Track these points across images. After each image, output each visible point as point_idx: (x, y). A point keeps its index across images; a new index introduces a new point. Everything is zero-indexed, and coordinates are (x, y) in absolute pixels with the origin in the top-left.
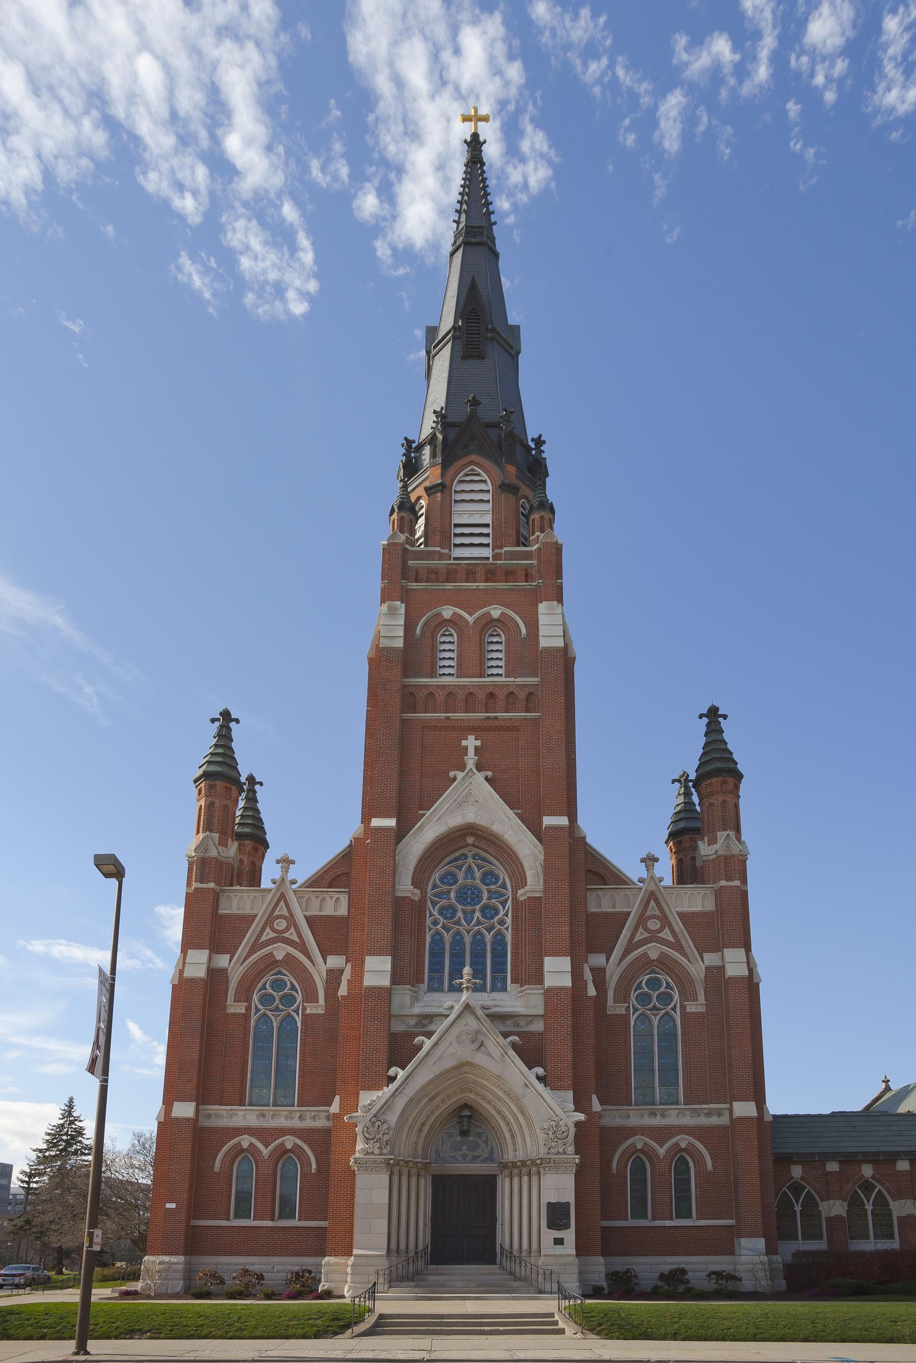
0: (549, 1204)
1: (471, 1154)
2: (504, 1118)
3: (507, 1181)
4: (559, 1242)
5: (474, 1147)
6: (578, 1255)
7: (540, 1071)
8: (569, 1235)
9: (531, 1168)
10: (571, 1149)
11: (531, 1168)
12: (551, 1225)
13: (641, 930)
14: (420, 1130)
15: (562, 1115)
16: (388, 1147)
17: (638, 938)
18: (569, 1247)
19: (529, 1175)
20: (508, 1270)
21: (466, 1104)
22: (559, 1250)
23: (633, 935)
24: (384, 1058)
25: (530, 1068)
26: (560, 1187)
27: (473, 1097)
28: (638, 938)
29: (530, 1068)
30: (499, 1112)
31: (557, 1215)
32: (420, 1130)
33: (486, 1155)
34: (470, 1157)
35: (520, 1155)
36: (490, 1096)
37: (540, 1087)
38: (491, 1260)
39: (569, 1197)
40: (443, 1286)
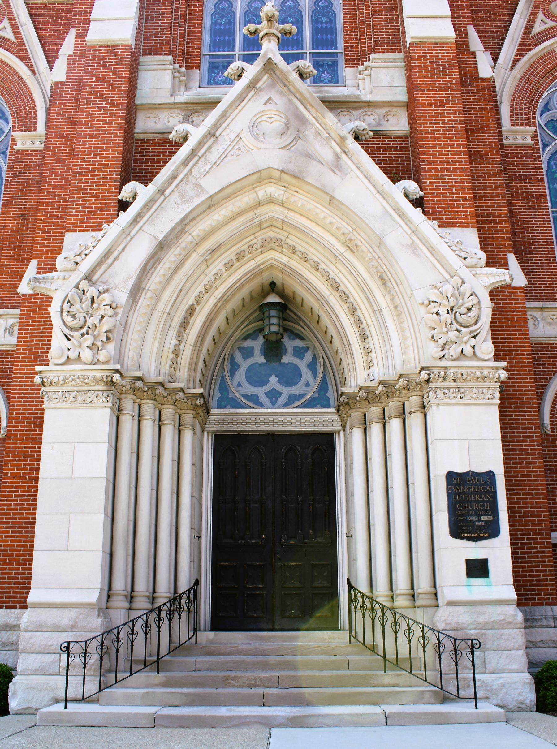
0: (451, 477)
1: (286, 391)
2: (345, 298)
3: (357, 435)
4: (478, 569)
5: (291, 377)
6: (523, 600)
7: (411, 185)
8: (498, 552)
9: (405, 396)
10: (487, 348)
11: (405, 396)
12: (459, 529)
13: (540, 16)
14: (184, 325)
15: (466, 273)
16: (111, 347)
17: (538, 28)
18: (501, 583)
19: (403, 415)
20: (369, 640)
21: (273, 284)
22: (479, 588)
23: (530, 24)
24: (115, 169)
25: (395, 181)
26: (469, 435)
27: (284, 259)
28: (538, 28)
29: (395, 181)
30: (335, 286)
31: (469, 504)
32: (184, 325)
33: (311, 392)
34: (283, 399)
35: (383, 371)
36: (315, 255)
37: (416, 214)
38: (338, 630)
39: (489, 458)
40: (225, 682)
